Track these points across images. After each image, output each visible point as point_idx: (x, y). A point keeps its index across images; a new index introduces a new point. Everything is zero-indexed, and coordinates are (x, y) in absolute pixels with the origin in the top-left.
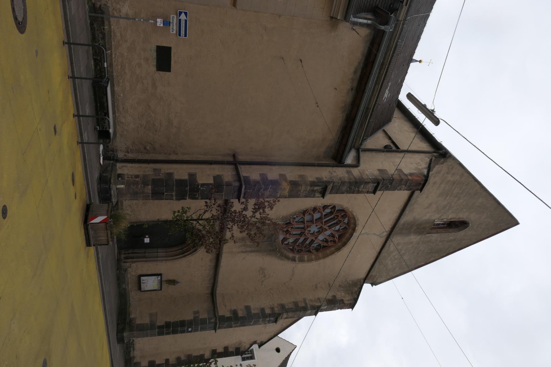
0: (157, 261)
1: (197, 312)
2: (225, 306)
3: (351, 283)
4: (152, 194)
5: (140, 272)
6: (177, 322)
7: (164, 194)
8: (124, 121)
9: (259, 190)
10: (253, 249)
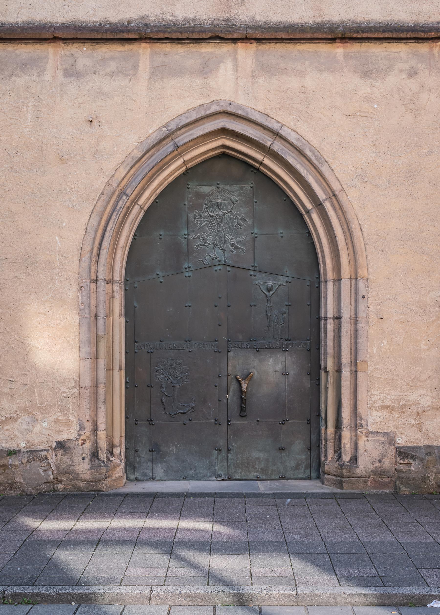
0: (355, 320)
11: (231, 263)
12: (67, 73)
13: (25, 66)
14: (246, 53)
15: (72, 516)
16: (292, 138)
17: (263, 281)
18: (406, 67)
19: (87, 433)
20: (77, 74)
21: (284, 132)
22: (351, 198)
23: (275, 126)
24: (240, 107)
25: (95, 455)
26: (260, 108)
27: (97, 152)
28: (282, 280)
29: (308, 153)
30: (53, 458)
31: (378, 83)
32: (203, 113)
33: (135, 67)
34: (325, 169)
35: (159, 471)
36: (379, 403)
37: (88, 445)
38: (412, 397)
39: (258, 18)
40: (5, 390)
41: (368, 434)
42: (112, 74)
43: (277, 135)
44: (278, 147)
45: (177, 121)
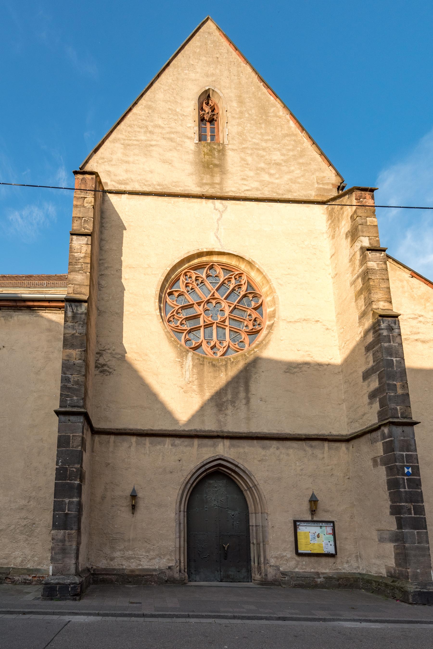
1: (374, 460)
2: (364, 415)
3: (330, 222)
4: (66, 529)
5: (290, 553)
6: (390, 493)
7: (67, 514)
8: (21, 559)
9: (69, 388)
11: (220, 506)
12: (172, 445)
13: (159, 443)
14: (227, 442)
15: (393, 572)
16: (242, 467)
17: (231, 512)
18: (276, 446)
19: (178, 564)
20: (175, 446)
21: (239, 465)
22: (261, 487)
23: (237, 463)
24: (225, 457)
25: (180, 571)
26: (232, 458)
27: (181, 470)
28: (237, 512)
29: (247, 472)
30: (167, 572)
31: (268, 451)
32: (214, 459)
33: (193, 444)
34: (252, 477)
35: (198, 578)
36: (274, 556)
37: (178, 568)
38: (285, 554)
39: (230, 430)
40: (152, 548)
41: (270, 566)
42: (186, 446)
43: (237, 466)
44: (237, 470)
45: (206, 461)
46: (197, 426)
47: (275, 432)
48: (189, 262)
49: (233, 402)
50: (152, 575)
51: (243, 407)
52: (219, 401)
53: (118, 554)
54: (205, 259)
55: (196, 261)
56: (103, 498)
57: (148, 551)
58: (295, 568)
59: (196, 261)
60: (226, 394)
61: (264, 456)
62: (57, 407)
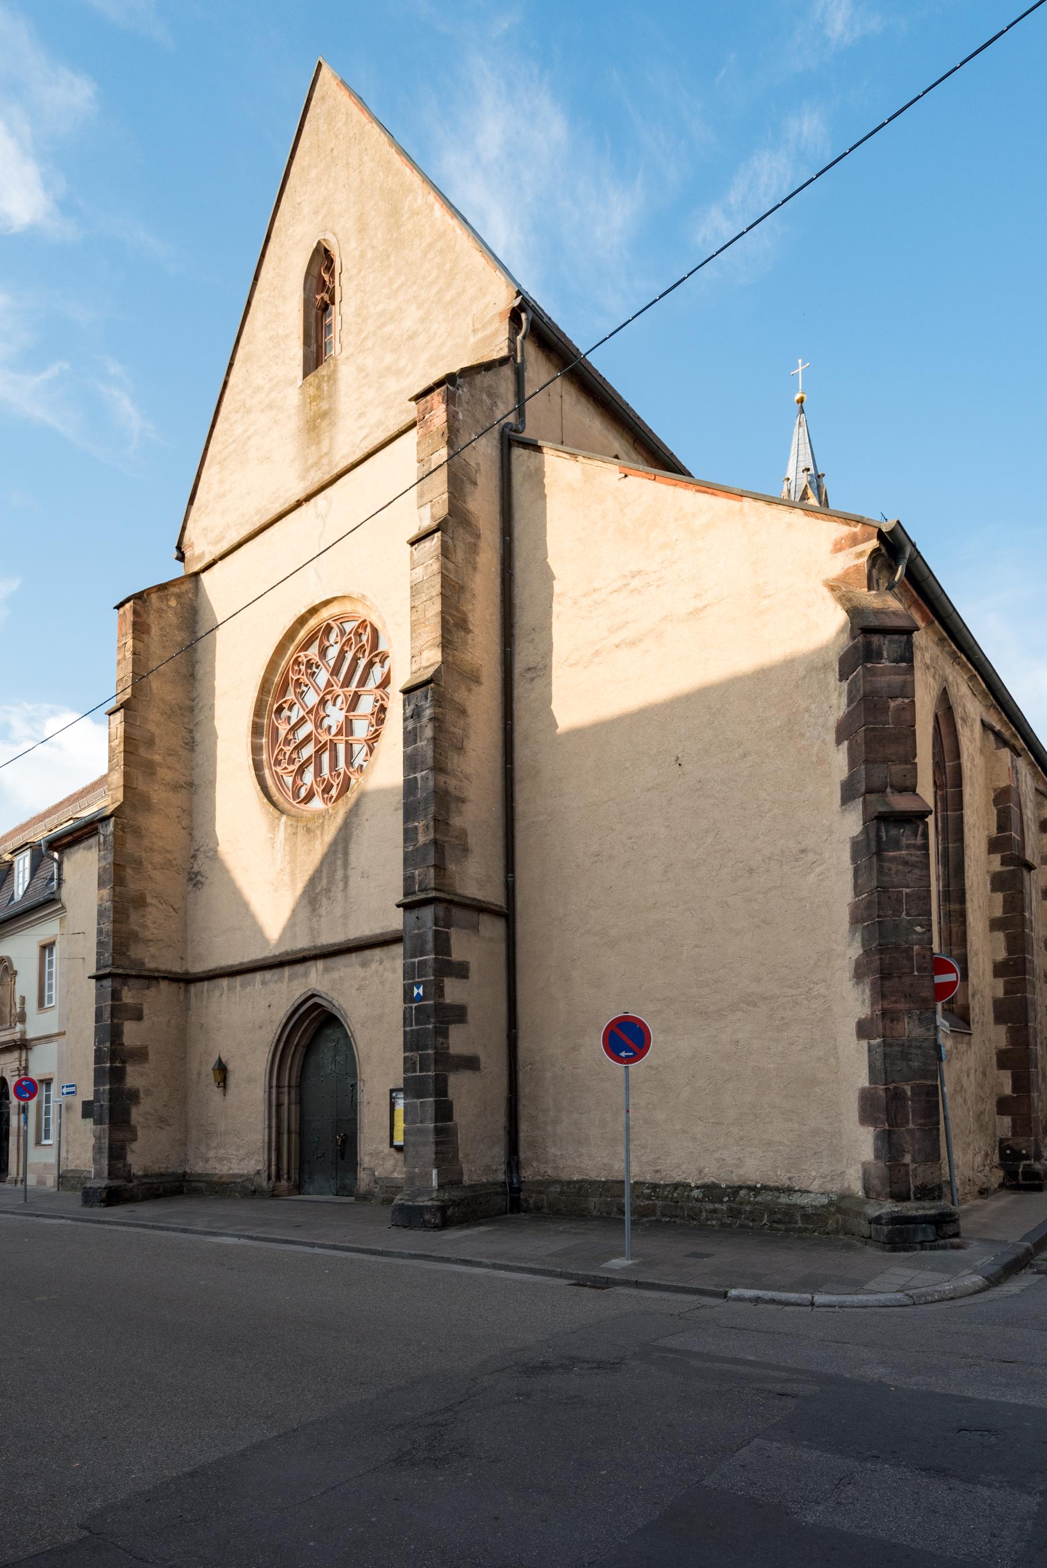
5: (386, 1149)
10: (339, 862)
14: (320, 964)
38: (381, 1149)
46: (302, 943)
47: (378, 931)
48: (293, 641)
49: (328, 890)
50: (235, 1183)
51: (340, 896)
52: (313, 895)
53: (212, 1154)
54: (313, 623)
55: (303, 634)
56: (199, 1074)
57: (237, 1150)
58: (393, 1172)
59: (303, 634)
60: (320, 878)
61: (364, 979)
62: (93, 971)
